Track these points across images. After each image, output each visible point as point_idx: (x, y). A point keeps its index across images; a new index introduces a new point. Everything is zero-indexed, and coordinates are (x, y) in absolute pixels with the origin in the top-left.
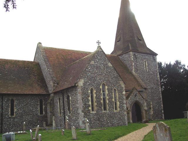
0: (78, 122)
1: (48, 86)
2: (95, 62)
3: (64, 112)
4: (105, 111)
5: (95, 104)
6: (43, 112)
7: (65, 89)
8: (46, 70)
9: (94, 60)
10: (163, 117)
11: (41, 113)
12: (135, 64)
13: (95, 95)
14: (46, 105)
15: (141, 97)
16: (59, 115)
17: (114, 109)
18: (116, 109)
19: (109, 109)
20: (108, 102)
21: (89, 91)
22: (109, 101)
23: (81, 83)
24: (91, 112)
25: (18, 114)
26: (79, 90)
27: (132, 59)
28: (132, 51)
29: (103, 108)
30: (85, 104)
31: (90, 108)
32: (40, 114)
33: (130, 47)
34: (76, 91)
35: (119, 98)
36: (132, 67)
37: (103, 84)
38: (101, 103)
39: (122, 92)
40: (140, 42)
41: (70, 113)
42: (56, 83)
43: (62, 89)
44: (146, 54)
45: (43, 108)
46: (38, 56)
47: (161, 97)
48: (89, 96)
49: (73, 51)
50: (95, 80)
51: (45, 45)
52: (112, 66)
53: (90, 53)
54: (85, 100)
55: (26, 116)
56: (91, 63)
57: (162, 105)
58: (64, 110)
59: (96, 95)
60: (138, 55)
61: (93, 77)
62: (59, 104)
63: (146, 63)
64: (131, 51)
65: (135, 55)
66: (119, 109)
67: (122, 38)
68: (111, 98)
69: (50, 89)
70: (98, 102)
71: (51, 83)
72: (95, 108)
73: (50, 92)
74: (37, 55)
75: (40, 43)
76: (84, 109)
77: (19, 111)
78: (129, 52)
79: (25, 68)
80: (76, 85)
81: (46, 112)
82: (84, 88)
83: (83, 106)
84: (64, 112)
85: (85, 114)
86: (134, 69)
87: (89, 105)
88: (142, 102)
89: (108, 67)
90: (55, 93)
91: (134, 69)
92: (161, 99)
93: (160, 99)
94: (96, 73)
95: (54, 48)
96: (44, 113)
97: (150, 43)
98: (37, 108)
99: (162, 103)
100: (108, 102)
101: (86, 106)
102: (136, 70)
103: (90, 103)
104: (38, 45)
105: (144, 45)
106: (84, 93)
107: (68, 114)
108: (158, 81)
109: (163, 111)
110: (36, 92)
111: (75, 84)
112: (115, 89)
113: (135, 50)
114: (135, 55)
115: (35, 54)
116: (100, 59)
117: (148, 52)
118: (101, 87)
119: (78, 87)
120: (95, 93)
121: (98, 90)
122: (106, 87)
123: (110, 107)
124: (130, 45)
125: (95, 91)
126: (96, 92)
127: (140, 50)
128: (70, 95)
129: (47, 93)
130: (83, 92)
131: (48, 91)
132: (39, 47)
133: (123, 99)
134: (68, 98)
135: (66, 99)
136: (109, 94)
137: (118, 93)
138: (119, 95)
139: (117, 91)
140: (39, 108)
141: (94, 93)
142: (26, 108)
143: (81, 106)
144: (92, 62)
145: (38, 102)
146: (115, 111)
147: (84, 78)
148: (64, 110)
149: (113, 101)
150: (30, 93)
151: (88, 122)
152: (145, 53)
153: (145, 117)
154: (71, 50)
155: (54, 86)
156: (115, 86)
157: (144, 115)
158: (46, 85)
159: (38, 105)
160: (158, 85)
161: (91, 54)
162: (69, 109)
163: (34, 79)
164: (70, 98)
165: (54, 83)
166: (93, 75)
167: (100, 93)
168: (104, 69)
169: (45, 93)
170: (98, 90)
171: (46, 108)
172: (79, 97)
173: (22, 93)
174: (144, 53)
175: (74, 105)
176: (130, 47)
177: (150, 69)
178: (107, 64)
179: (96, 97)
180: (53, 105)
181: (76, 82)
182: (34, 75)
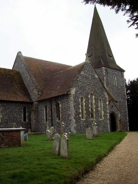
0: (70, 128)
1: (30, 94)
2: (84, 73)
3: (52, 119)
4: (92, 119)
5: (85, 112)
6: (26, 119)
7: (54, 97)
8: (28, 79)
9: (84, 71)
10: (128, 129)
11: (25, 120)
12: (106, 78)
13: (84, 104)
14: (30, 113)
15: (116, 108)
16: (45, 122)
17: (99, 117)
18: (101, 118)
19: (95, 117)
20: (94, 110)
21: (80, 100)
22: (96, 110)
23: (73, 91)
24: (81, 119)
25: (3, 120)
26: (72, 98)
27: (104, 74)
28: (104, 66)
29: (91, 116)
30: (77, 112)
31: (80, 116)
32: (24, 121)
33: (103, 63)
34: (68, 98)
35: (104, 108)
36: (104, 80)
37: (91, 93)
38: (89, 111)
39: (106, 102)
40: (111, 58)
41: (59, 119)
42: (40, 92)
43: (49, 97)
44: (116, 70)
45: (27, 115)
46: (18, 64)
47: (127, 110)
48: (79, 104)
49: (50, 62)
50: (84, 90)
51: (25, 54)
52: (98, 77)
53: (71, 66)
54: (76, 107)
55: (11, 123)
56: (81, 73)
57: (128, 118)
58: (52, 117)
59: (86, 104)
60: (110, 71)
61: (83, 87)
62: (45, 112)
63: (116, 79)
64: (103, 66)
65: (106, 70)
66: (103, 118)
67: (94, 53)
68: (97, 107)
69: (33, 97)
70: (87, 110)
71: (35, 92)
72: (85, 116)
73: (34, 100)
74: (17, 64)
75: (20, 52)
76: (76, 116)
77: (4, 117)
78: (102, 66)
79: (7, 76)
80: (69, 93)
81: (30, 120)
82: (75, 96)
83: (75, 114)
84: (52, 119)
85: (76, 120)
86: (105, 83)
87: (80, 112)
88: (117, 113)
89: (95, 78)
90: (40, 102)
91: (105, 83)
92: (127, 112)
93: (126, 112)
94: (85, 83)
95: (32, 58)
96: (27, 120)
97: (120, 62)
98: (21, 115)
99: (127, 116)
100: (94, 110)
101: (77, 114)
102: (108, 84)
103: (81, 111)
104: (18, 55)
105: (114, 62)
106: (76, 101)
107: (57, 121)
108: (125, 96)
109: (128, 124)
110: (20, 100)
111: (68, 92)
112: (100, 99)
113: (107, 66)
114: (106, 70)
115: (15, 62)
116: (89, 70)
117: (118, 68)
118: (89, 96)
119: (70, 95)
120: (85, 102)
121: (87, 100)
122: (94, 97)
123: (96, 116)
124: (102, 60)
125: (85, 100)
126: (86, 101)
127: (111, 65)
128: (60, 102)
129: (31, 101)
130: (75, 100)
131: (31, 99)
132: (19, 56)
133: (106, 109)
134: (57, 105)
135: (54, 107)
136: (95, 103)
137: (103, 102)
138: (103, 105)
139: (102, 101)
140: (23, 116)
141: (84, 102)
142: (10, 114)
143: (73, 113)
144: (82, 73)
145: (22, 110)
146: (100, 119)
147: (76, 86)
148: (52, 117)
149: (98, 110)
150: (15, 100)
151: (96, 125)
152: (115, 69)
153: (119, 127)
154: (48, 62)
155: (38, 94)
156: (100, 96)
157: (119, 125)
158: (29, 94)
159: (22, 112)
160: (124, 99)
161: (72, 68)
162: (58, 116)
163: (17, 87)
164: (60, 106)
165: (39, 92)
166: (83, 85)
167: (88, 101)
168: (92, 80)
169: (28, 101)
170: (87, 100)
171: (30, 116)
172: (72, 104)
173: (8, 100)
174: (114, 69)
175: (65, 112)
176: (103, 63)
177: (118, 84)
178: (94, 76)
179: (85, 105)
180: (37, 112)
181: (68, 90)
182: (16, 83)
